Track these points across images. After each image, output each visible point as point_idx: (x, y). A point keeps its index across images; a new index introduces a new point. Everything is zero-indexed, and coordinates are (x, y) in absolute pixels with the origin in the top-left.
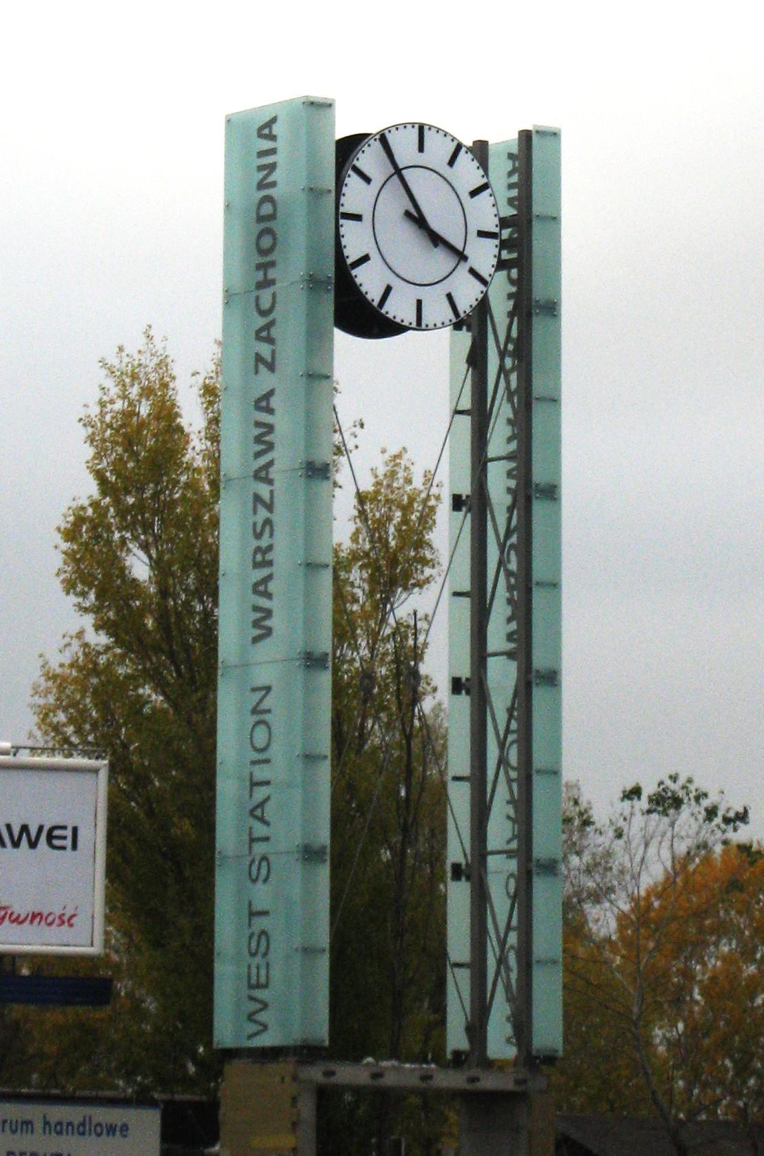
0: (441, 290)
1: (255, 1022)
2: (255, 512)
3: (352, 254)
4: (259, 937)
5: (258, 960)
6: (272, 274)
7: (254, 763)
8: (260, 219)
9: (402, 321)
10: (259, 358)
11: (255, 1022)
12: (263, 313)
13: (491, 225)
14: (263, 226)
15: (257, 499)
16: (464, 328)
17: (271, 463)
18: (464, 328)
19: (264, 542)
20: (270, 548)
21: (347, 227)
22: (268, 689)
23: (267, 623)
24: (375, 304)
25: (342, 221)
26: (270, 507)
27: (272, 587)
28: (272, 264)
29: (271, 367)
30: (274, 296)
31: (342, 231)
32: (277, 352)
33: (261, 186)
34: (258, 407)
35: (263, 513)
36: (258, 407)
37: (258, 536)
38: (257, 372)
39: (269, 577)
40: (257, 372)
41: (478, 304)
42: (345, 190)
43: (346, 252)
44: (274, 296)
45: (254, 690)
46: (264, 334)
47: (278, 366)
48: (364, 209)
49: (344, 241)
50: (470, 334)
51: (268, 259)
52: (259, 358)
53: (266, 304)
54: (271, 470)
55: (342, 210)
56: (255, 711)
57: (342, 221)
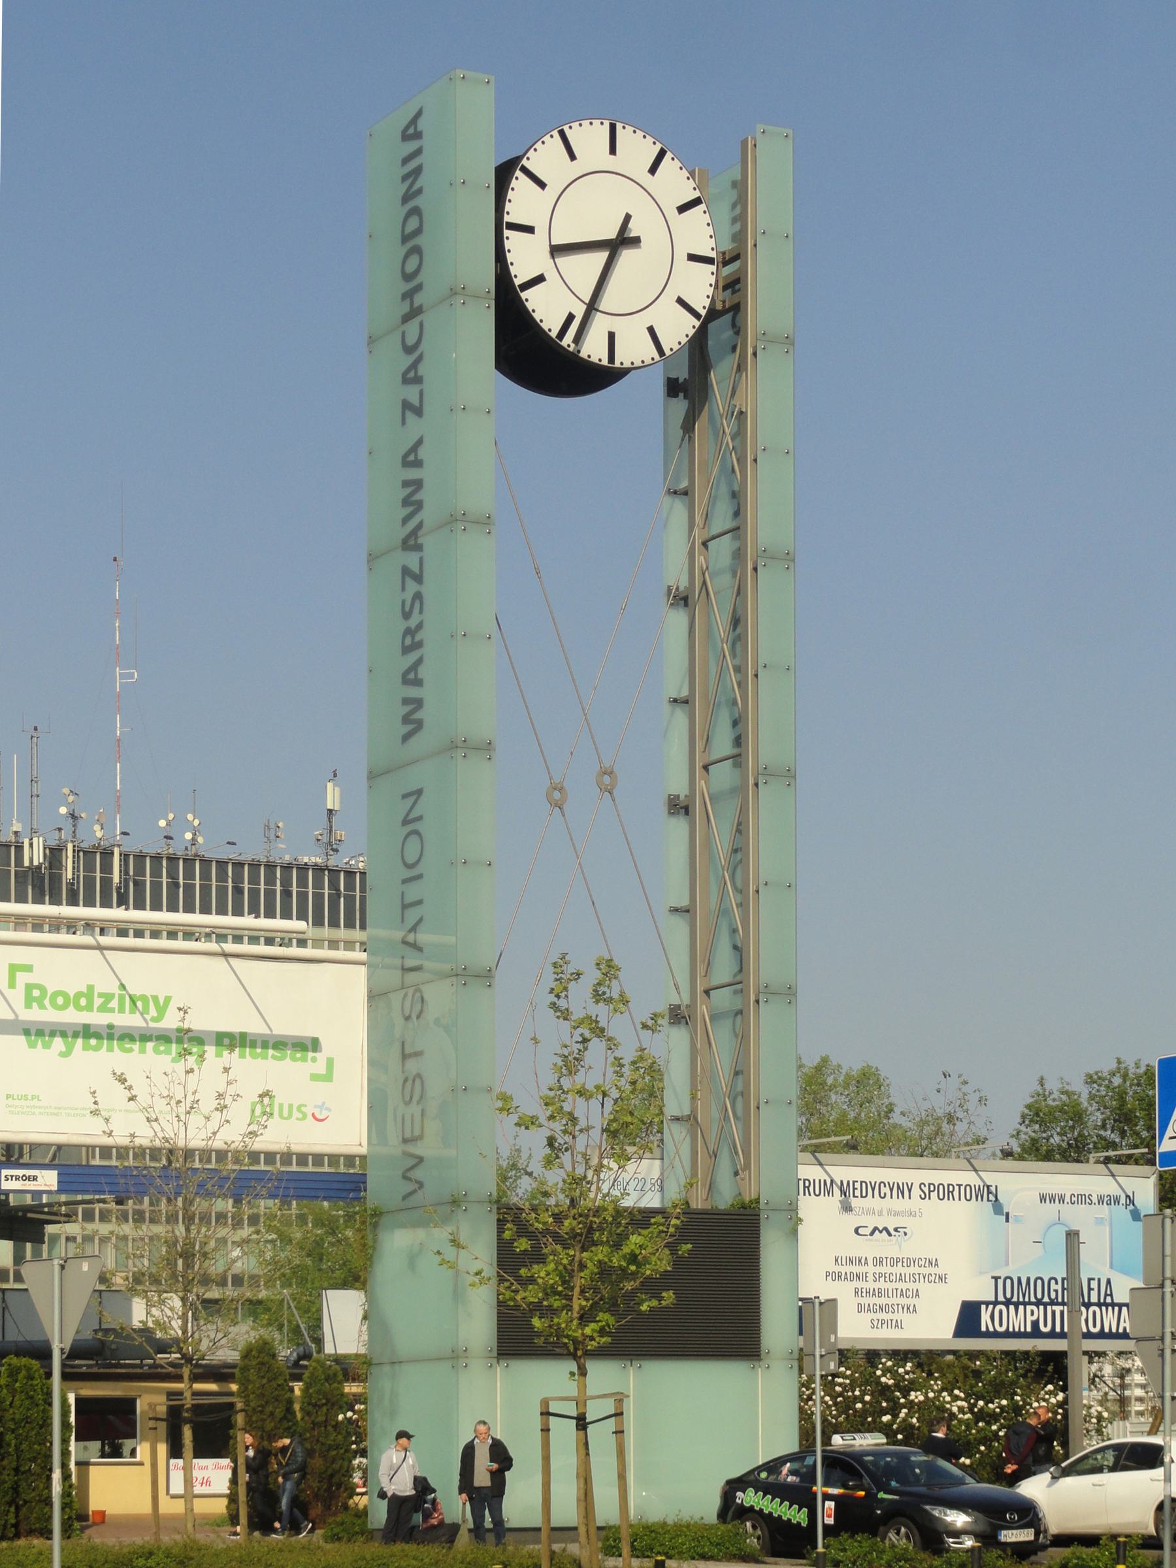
0: (641, 322)
1: (410, 1179)
2: (403, 589)
3: (520, 273)
4: (414, 1081)
5: (415, 1109)
6: (418, 299)
7: (404, 881)
8: (405, 239)
9: (591, 123)
10: (406, 405)
11: (410, 1179)
12: (409, 866)
13: (706, 248)
14: (409, 245)
15: (406, 571)
16: (681, 395)
17: (420, 526)
18: (681, 395)
19: (413, 622)
20: (420, 626)
21: (513, 240)
22: (419, 792)
23: (417, 716)
24: (554, 334)
25: (507, 233)
26: (418, 578)
27: (423, 672)
28: (419, 288)
29: (418, 411)
30: (421, 325)
31: (508, 245)
32: (425, 560)
33: (406, 199)
34: (406, 681)
35: (412, 586)
36: (406, 681)
37: (407, 615)
38: (404, 422)
39: (420, 661)
40: (404, 422)
41: (688, 341)
42: (510, 195)
43: (513, 270)
44: (421, 325)
45: (405, 796)
46: (412, 374)
47: (426, 409)
48: (538, 220)
49: (510, 258)
50: (687, 401)
51: (409, 245)
52: (406, 405)
53: (410, 341)
54: (420, 533)
55: (507, 219)
56: (405, 822)
57: (507, 233)
